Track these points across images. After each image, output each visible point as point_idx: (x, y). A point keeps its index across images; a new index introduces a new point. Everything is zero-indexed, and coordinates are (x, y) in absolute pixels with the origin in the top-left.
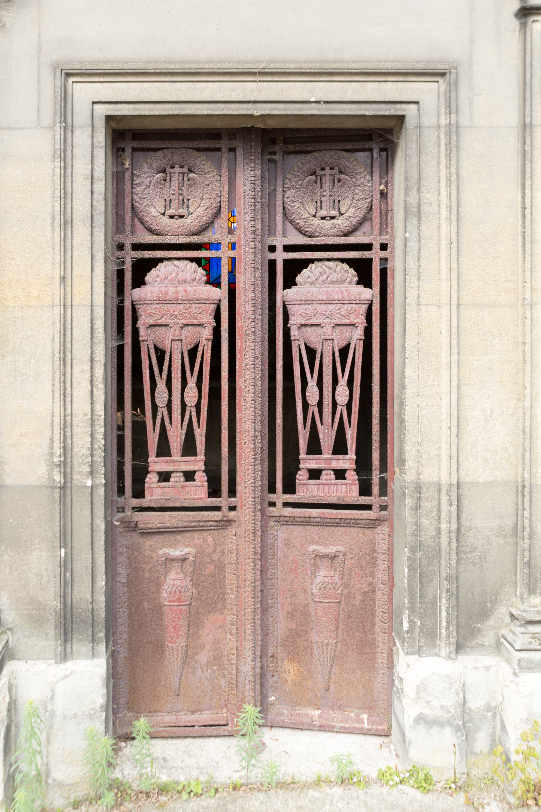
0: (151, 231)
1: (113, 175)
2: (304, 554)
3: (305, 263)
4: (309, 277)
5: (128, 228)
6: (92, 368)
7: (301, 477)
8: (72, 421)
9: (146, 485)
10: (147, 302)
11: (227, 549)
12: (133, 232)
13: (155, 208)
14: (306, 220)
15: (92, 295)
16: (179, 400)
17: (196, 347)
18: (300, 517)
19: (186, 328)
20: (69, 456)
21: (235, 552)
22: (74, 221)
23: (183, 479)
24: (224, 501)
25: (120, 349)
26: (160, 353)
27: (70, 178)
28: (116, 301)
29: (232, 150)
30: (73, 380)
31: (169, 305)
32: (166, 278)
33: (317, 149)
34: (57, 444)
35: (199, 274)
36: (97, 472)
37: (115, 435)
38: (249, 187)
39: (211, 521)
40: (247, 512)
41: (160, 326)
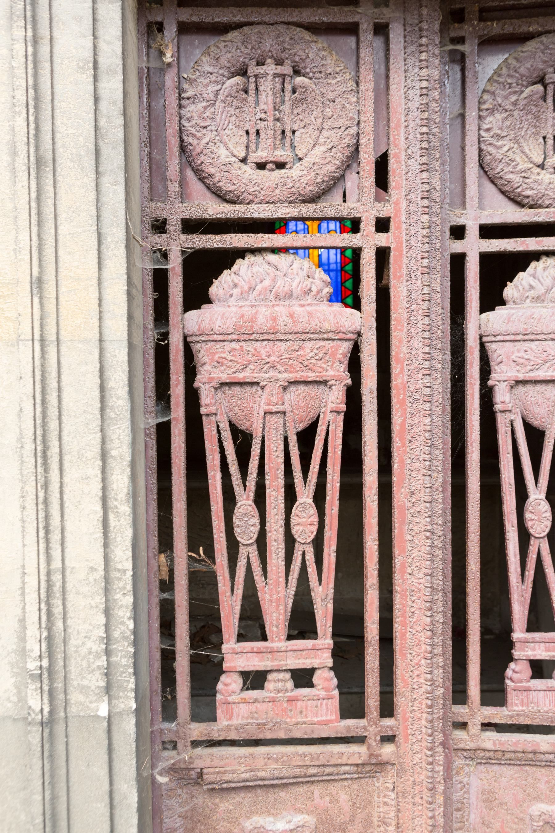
0: (219, 196)
1: (140, 79)
2: (522, 819)
3: (521, 261)
4: (531, 287)
5: (174, 187)
6: (104, 471)
7: (516, 676)
8: (64, 582)
9: (219, 697)
10: (215, 337)
11: (376, 814)
12: (183, 196)
13: (227, 149)
14: (525, 175)
15: (100, 318)
16: (282, 530)
17: (313, 427)
18: (514, 752)
19: (293, 388)
20: (59, 656)
21: (394, 823)
22: (59, 161)
23: (290, 684)
24: (369, 725)
25: (163, 432)
26: (243, 440)
27: (47, 65)
28: (152, 335)
29: (381, 30)
30: (65, 497)
31: (258, 344)
32: (252, 289)
33: (547, 28)
34: (33, 632)
35: (317, 282)
36: (120, 687)
37: (155, 601)
38: (417, 102)
39: (346, 765)
40: (416, 747)
41: (241, 384)
